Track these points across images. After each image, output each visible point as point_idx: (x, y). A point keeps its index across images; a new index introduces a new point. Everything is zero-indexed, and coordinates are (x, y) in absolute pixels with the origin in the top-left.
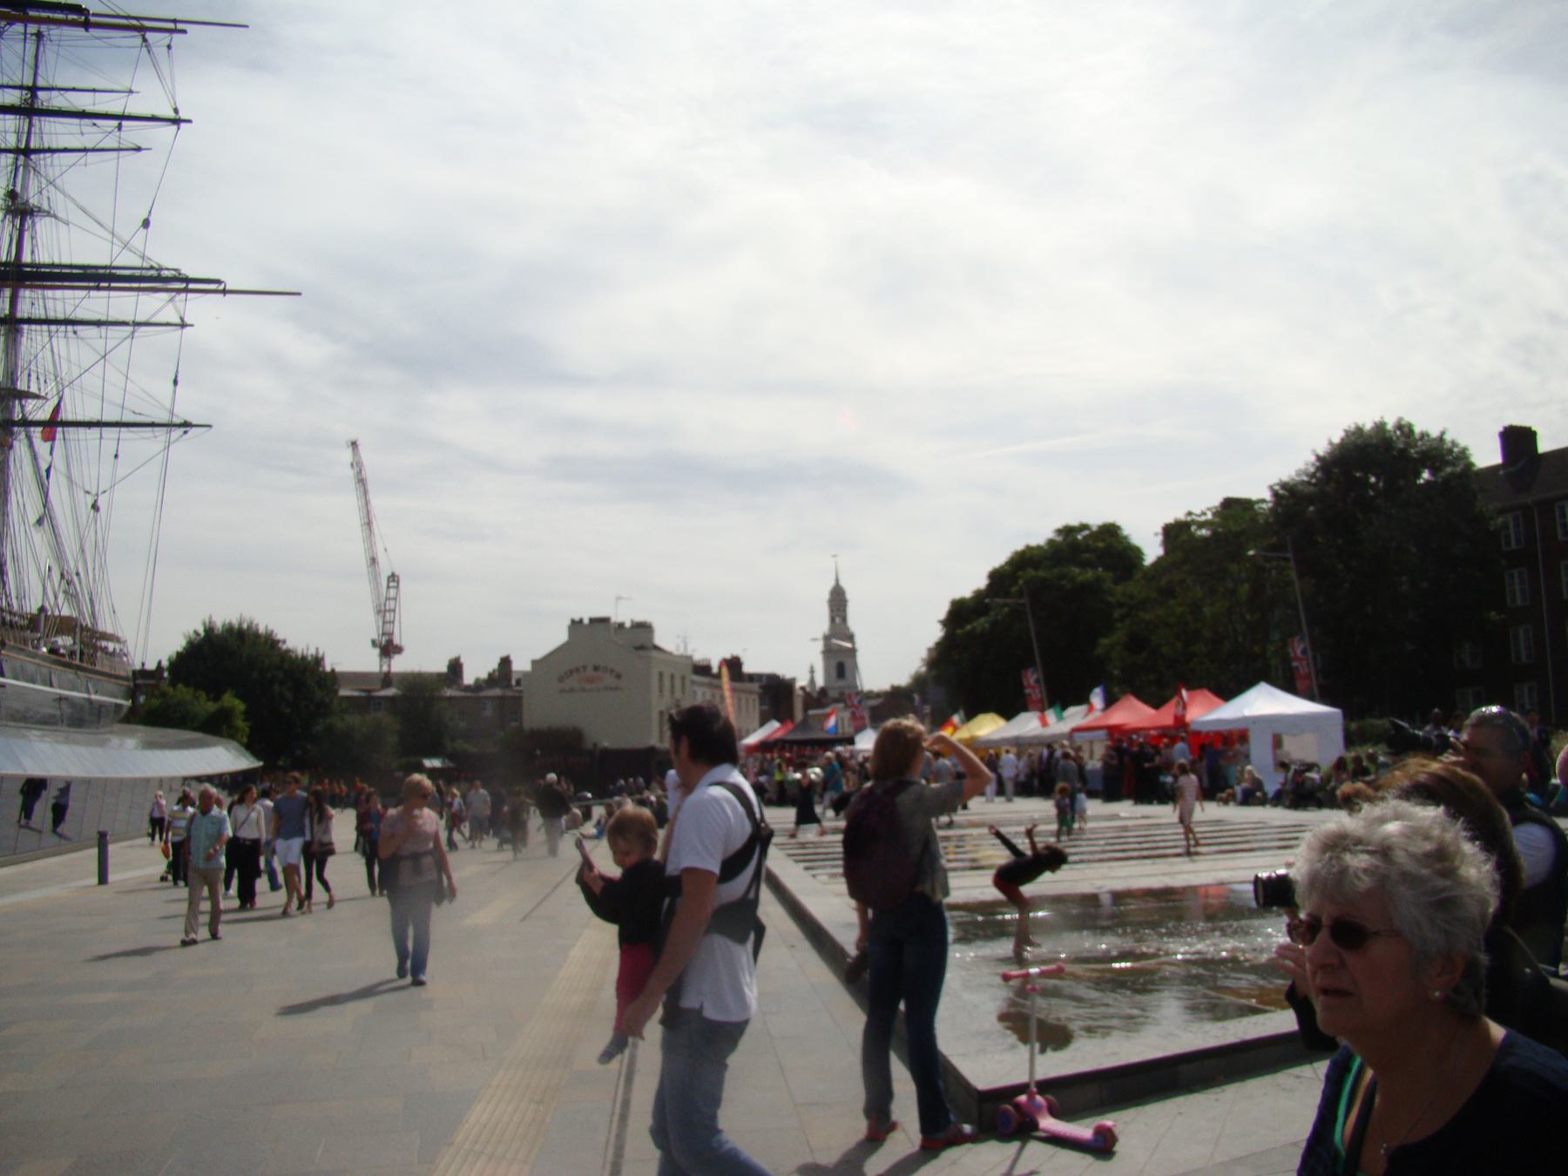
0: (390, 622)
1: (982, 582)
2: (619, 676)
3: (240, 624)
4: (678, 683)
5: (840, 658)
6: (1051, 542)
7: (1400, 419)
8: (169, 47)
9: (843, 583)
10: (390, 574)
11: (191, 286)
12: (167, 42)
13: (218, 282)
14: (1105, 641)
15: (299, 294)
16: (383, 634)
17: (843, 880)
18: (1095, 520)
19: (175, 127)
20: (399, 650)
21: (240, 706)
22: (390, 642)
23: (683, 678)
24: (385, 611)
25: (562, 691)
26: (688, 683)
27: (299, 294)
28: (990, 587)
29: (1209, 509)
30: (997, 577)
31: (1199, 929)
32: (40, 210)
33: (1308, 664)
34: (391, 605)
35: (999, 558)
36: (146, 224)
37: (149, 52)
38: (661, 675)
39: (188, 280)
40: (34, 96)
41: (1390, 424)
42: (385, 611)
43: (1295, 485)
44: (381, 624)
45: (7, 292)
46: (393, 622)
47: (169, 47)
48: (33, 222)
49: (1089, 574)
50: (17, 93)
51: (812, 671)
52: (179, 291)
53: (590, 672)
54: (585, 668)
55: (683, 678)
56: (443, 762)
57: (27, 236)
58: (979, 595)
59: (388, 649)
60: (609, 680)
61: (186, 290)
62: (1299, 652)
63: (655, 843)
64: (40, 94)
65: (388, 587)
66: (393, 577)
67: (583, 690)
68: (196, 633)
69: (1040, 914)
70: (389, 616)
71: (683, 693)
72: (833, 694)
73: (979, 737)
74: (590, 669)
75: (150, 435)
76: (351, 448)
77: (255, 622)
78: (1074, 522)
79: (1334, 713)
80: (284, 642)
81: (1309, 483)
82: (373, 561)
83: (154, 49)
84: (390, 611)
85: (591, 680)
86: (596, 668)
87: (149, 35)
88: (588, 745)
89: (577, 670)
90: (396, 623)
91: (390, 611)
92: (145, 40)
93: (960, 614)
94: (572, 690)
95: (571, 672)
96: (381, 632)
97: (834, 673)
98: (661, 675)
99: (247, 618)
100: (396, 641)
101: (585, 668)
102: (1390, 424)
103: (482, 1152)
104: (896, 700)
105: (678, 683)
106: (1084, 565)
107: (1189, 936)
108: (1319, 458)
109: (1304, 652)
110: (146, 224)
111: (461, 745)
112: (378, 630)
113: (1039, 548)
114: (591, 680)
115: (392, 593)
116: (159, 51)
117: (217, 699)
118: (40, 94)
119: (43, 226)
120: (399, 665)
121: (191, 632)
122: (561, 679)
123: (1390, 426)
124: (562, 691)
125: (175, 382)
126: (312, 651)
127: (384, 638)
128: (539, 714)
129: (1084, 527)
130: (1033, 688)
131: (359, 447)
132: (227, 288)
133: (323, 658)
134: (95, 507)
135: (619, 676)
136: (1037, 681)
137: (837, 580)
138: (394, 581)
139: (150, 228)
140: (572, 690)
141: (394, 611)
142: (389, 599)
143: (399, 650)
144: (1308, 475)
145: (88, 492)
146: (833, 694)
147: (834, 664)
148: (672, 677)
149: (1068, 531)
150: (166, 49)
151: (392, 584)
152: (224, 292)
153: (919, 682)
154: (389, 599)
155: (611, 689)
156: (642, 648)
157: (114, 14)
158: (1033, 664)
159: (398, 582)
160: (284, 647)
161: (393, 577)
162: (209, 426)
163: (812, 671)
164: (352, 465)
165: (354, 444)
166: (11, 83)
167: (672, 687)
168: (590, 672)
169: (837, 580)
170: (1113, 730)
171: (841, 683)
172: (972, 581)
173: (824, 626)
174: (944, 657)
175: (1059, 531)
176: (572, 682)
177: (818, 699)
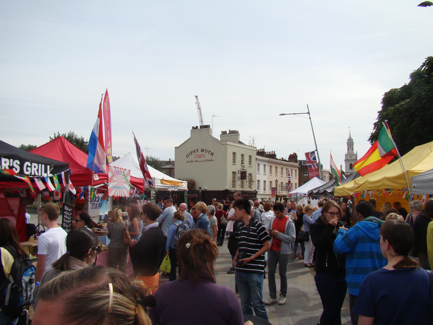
2: (212, 154)
4: (246, 159)
15: (307, 105)
17: (345, 297)
23: (250, 157)
25: (188, 162)
26: (253, 159)
27: (307, 105)
31: (271, 214)
51: (341, 167)
53: (200, 153)
55: (250, 157)
56: (239, 261)
60: (209, 157)
67: (196, 161)
69: (209, 226)
74: (200, 151)
85: (200, 156)
86: (202, 150)
89: (194, 152)
94: (192, 161)
97: (349, 167)
101: (197, 150)
105: (246, 159)
107: (188, 198)
114: (200, 156)
122: (187, 156)
124: (188, 162)
135: (212, 154)
137: (350, 136)
140: (192, 161)
147: (349, 164)
148: (242, 155)
155: (209, 161)
164: (196, 103)
165: (196, 97)
168: (200, 153)
169: (350, 136)
173: (345, 151)
176: (191, 158)
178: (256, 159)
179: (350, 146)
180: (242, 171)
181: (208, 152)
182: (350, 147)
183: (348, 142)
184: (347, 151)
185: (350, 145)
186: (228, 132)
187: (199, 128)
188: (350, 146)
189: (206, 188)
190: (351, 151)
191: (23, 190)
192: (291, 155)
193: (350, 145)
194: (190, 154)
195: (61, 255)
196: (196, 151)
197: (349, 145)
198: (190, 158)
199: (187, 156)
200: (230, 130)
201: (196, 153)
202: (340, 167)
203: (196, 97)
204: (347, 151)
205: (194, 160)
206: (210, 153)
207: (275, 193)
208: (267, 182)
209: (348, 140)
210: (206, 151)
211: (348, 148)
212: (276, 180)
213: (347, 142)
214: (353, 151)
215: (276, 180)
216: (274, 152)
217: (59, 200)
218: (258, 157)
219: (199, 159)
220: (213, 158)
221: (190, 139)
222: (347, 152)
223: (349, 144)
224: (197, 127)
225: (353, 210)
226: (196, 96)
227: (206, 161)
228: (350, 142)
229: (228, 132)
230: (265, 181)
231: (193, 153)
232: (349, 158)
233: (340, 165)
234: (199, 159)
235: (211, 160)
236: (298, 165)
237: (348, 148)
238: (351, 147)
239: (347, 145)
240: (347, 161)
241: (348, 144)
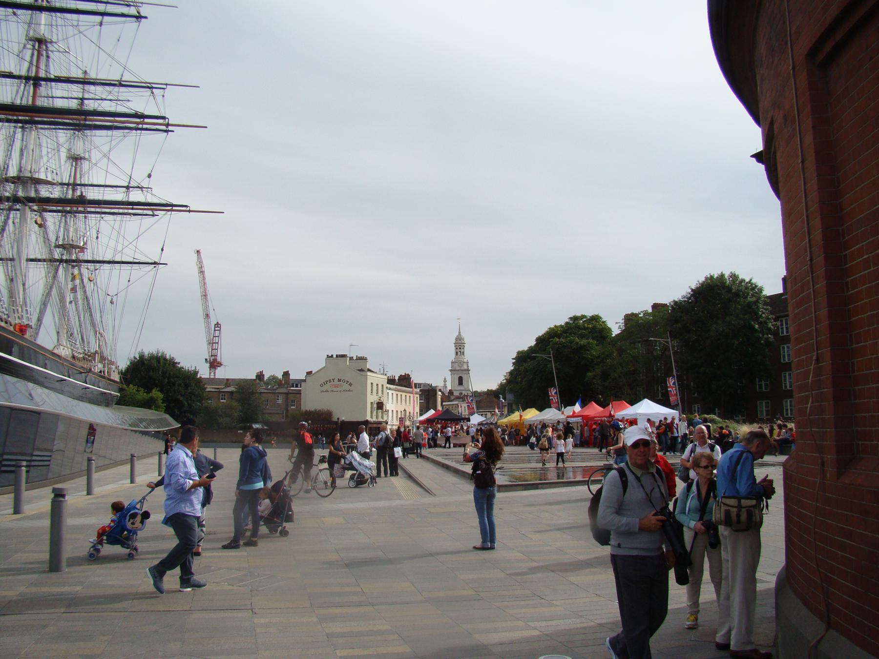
0: (215, 349)
1: (533, 343)
2: (351, 385)
3: (158, 353)
5: (461, 374)
6: (567, 323)
7: (731, 273)
8: (163, 96)
9: (463, 335)
10: (216, 323)
11: (174, 208)
12: (162, 94)
13: (186, 206)
14: (589, 374)
16: (212, 356)
18: (589, 313)
19: (166, 134)
20: (220, 364)
21: (160, 395)
22: (215, 360)
23: (382, 385)
24: (213, 343)
26: (385, 387)
28: (536, 345)
29: (641, 312)
30: (540, 340)
32: (84, 159)
33: (676, 389)
34: (216, 339)
35: (541, 331)
36: (149, 176)
37: (154, 98)
38: (372, 383)
39: (173, 205)
40: (82, 104)
41: (727, 275)
42: (213, 343)
43: (681, 303)
44: (210, 350)
45: (594, 493)
46: (217, 349)
47: (163, 96)
48: (81, 164)
49: (584, 342)
50: (76, 101)
51: (445, 381)
52: (168, 210)
53: (336, 382)
54: (333, 380)
55: (382, 385)
57: (78, 170)
58: (531, 350)
59: (214, 364)
60: (346, 387)
61: (172, 210)
62: (671, 384)
63: (111, 603)
64: (86, 102)
65: (215, 330)
66: (218, 325)
67: (332, 391)
68: (135, 358)
70: (215, 346)
71: (382, 393)
72: (456, 394)
73: (526, 419)
74: (336, 380)
75: (138, 268)
76: (196, 254)
77: (165, 353)
78: (579, 314)
79: (675, 413)
80: (179, 363)
81: (688, 301)
82: (207, 316)
83: (157, 97)
84: (215, 343)
85: (337, 386)
86: (339, 380)
87: (154, 90)
88: (335, 419)
89: (330, 381)
90: (219, 350)
91: (215, 343)
92: (152, 93)
93: (522, 358)
94: (327, 391)
95: (327, 382)
96: (210, 355)
97: (457, 382)
98: (372, 383)
99: (161, 351)
100: (219, 360)
101: (333, 380)
102: (727, 275)
103: (482, 396)
104: (492, 395)
106: (582, 336)
108: (692, 290)
109: (674, 384)
110: (149, 176)
111: (268, 417)
112: (209, 353)
113: (561, 326)
114: (337, 386)
115: (217, 333)
116: (159, 98)
117: (149, 391)
118: (86, 102)
119: (85, 165)
120: (221, 373)
121: (132, 357)
122: (322, 385)
123: (726, 276)
125: (162, 250)
126: (193, 368)
127: (212, 358)
128: (311, 401)
129: (583, 316)
130: (554, 396)
131: (201, 254)
132: (191, 209)
133: (198, 372)
134: (112, 302)
135: (351, 385)
136: (556, 393)
137: (459, 332)
138: (218, 327)
139: (151, 178)
140: (327, 391)
141: (218, 343)
142: (215, 337)
143: (220, 364)
144: (687, 298)
145: (108, 295)
146: (456, 394)
149: (575, 319)
150: (162, 97)
151: (216, 329)
152: (189, 211)
153: (502, 389)
154: (215, 337)
155: (347, 391)
156: (362, 370)
157: (139, 81)
158: (553, 386)
159: (220, 327)
160: (179, 366)
161: (218, 325)
162: (166, 264)
163: (445, 381)
165: (198, 252)
166: (73, 96)
167: (377, 390)
168: (336, 382)
169: (459, 332)
170: (584, 417)
171: (461, 388)
172: (528, 342)
173: (452, 356)
174: (513, 378)
175: (571, 318)
176: (327, 387)
177: (448, 396)
178: (387, 388)
179: (460, 348)
180: (378, 401)
181: (346, 382)
182: (460, 350)
183: (457, 342)
184: (454, 356)
185: (460, 347)
186: (355, 358)
187: (335, 356)
188: (460, 348)
189: (343, 419)
190: (460, 357)
191: (464, 445)
192: (401, 375)
193: (460, 347)
194: (325, 383)
195: (400, 466)
196: (332, 381)
197: (458, 348)
198: (325, 388)
199: (322, 385)
200: (357, 356)
201: (332, 383)
202: (444, 381)
203: (198, 252)
204: (454, 357)
205: (329, 389)
206: (348, 383)
207: (403, 423)
208: (394, 411)
209: (456, 339)
210: (344, 381)
211: (457, 352)
212: (405, 410)
213: (454, 341)
214: (463, 357)
215: (405, 410)
216: (394, 376)
217: (508, 451)
218: (389, 386)
219: (335, 389)
220: (352, 388)
221: (324, 367)
222: (455, 358)
223: (458, 345)
224: (332, 356)
225: (208, 403)
226: (197, 251)
227: (344, 391)
228: (460, 342)
229: (355, 358)
230: (392, 411)
231: (328, 383)
232: (458, 368)
233: (444, 378)
234: (335, 389)
235: (349, 391)
236: (419, 391)
237: (457, 352)
238: (462, 351)
239: (455, 346)
240: (454, 372)
241: (456, 345)
